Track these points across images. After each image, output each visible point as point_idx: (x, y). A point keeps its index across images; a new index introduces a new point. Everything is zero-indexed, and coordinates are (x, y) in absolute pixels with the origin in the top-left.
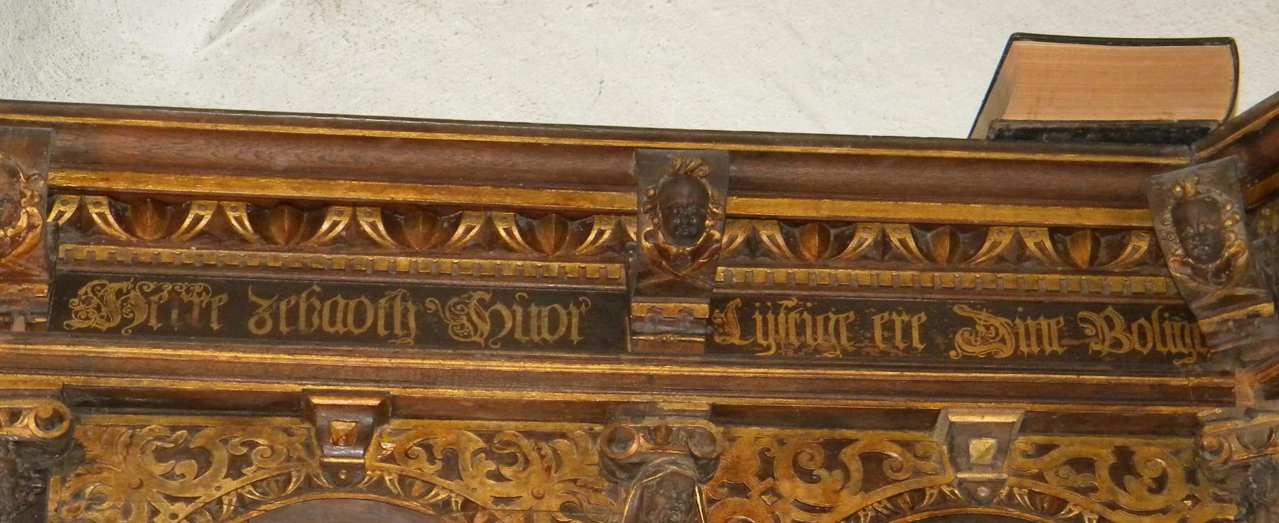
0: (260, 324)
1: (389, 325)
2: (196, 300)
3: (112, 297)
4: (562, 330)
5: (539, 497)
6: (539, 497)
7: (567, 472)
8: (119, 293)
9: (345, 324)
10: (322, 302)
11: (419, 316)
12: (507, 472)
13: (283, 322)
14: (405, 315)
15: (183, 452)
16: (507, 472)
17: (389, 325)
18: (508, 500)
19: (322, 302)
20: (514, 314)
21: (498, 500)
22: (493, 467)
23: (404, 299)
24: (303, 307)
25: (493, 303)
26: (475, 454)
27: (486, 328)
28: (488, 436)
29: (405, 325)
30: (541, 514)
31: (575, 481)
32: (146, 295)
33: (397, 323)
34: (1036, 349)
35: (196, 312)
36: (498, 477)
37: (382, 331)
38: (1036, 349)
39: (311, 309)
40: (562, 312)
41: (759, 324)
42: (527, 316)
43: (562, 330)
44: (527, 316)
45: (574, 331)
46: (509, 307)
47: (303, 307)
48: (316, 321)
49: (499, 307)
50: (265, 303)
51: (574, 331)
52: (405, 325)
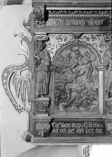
0: (67, 24)
1: (82, 23)
2: (60, 21)
3: (51, 21)
4: (101, 23)
5: (98, 43)
6: (98, 43)
7: (101, 40)
8: (52, 20)
9: (77, 24)
10: (74, 21)
11: (85, 22)
12: (94, 40)
13: (70, 23)
14: (83, 22)
15: (60, 38)
16: (94, 40)
17: (82, 23)
18: (95, 44)
19: (74, 21)
20: (95, 21)
21: (93, 44)
22: (93, 39)
23: (83, 20)
24: (72, 21)
25: (93, 20)
26: (91, 38)
27: (92, 23)
28: (92, 36)
29: (83, 23)
30: (32, 72)
31: (101, 41)
32: (55, 21)
33: (83, 23)
34: (92, 127)
35: (60, 22)
36: (93, 41)
37: (81, 24)
38: (92, 127)
39: (73, 22)
40: (101, 21)
41: (102, 23)
42: (97, 21)
43: (101, 23)
44: (97, 21)
45: (102, 24)
46: (95, 20)
47: (72, 21)
48: (74, 23)
49: (94, 20)
50: (68, 21)
51: (102, 24)
52: (83, 23)
